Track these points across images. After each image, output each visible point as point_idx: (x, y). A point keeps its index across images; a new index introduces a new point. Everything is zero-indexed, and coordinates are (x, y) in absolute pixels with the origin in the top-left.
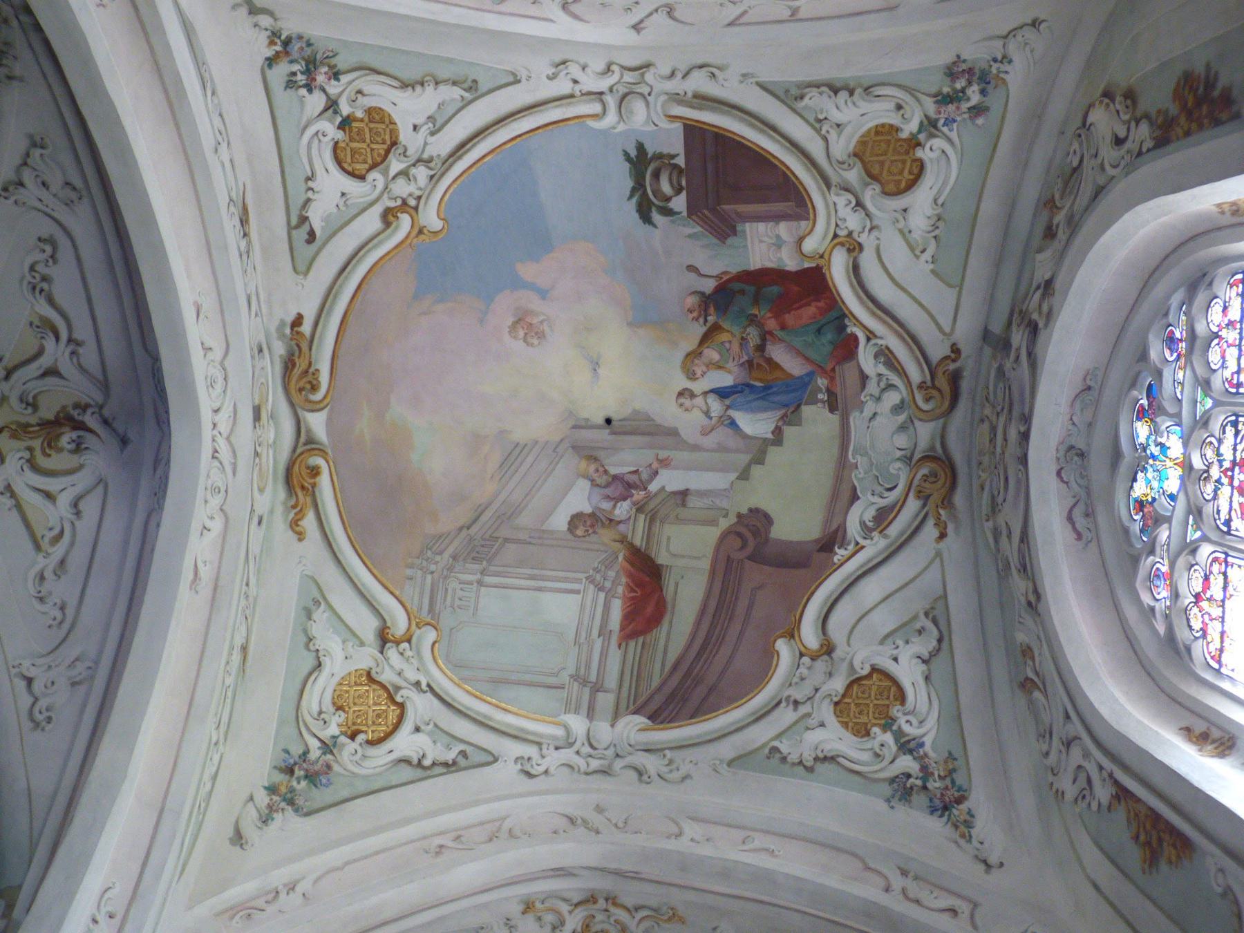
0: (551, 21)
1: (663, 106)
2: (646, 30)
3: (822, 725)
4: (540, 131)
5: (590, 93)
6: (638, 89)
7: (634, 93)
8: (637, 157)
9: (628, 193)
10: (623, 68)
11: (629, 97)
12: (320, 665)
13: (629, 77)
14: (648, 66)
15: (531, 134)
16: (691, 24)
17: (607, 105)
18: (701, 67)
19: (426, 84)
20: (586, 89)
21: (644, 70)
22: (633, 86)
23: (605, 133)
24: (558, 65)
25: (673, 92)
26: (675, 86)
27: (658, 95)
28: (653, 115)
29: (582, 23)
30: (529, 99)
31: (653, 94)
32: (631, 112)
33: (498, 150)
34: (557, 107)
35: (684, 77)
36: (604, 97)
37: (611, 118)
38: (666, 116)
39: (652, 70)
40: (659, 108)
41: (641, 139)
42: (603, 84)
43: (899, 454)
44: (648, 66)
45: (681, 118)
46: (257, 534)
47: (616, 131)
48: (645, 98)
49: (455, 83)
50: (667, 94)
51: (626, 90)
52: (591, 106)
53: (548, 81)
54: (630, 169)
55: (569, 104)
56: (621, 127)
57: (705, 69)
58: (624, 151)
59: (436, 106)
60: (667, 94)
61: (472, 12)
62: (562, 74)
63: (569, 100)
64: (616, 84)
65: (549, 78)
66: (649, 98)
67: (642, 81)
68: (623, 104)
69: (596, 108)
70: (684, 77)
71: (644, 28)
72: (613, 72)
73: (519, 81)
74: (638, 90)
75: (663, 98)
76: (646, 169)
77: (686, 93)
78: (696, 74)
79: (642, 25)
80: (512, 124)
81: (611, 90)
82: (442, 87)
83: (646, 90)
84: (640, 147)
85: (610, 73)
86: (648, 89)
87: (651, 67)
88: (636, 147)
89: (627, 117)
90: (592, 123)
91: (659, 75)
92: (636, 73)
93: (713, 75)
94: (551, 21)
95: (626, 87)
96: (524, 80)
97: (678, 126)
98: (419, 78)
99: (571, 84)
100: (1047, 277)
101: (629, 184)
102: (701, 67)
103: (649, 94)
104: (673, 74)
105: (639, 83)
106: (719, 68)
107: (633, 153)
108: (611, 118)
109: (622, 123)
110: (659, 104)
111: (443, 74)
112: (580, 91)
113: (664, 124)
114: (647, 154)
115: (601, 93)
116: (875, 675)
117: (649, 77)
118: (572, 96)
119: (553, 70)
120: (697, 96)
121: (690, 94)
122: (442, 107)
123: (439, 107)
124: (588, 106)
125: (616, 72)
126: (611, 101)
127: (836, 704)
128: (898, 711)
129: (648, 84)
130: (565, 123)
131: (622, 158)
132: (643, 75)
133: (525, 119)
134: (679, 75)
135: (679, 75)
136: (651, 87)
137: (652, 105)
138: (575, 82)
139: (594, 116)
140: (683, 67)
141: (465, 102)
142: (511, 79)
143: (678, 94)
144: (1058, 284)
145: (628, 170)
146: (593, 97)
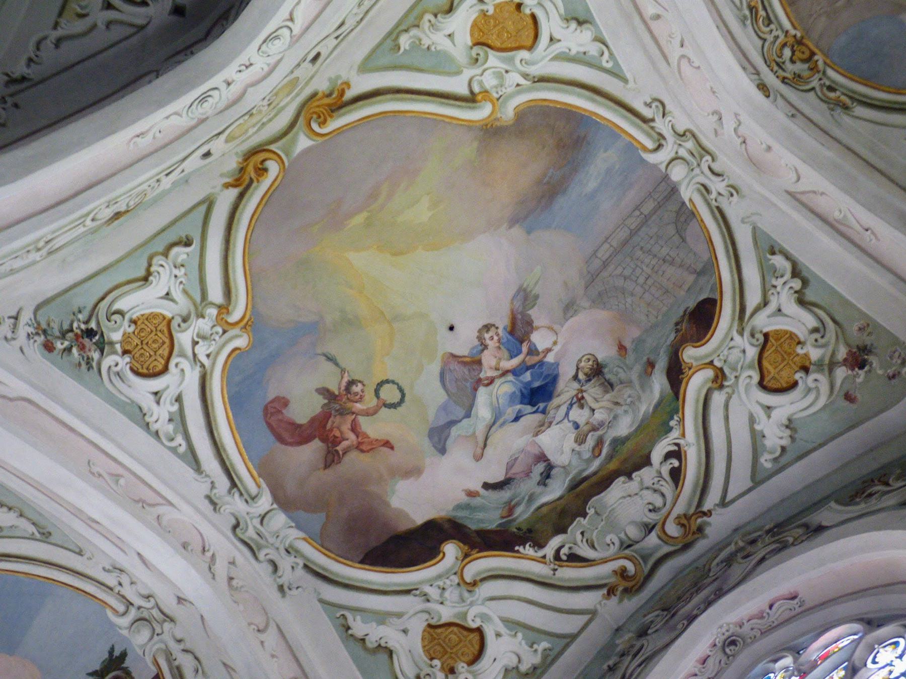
0: (125, 552)
1: (158, 649)
2: (183, 607)
3: (405, 631)
4: (72, 589)
5: (123, 597)
6: (155, 624)
7: (150, 623)
8: (116, 657)
9: (90, 671)
10: (157, 605)
11: (145, 622)
12: (146, 279)
13: (155, 612)
14: (172, 620)
15: (64, 585)
16: (208, 636)
17: (127, 614)
18: (196, 658)
19: (12, 511)
20: (123, 592)
21: (168, 619)
22: (153, 620)
23: (112, 625)
24: (115, 568)
25: (171, 650)
26: (175, 648)
27: (162, 641)
28: (148, 647)
29: (147, 569)
30: (79, 567)
31: (160, 637)
32: (139, 631)
33: (31, 577)
34: (96, 586)
35: (184, 650)
36: (131, 607)
37: (124, 622)
38: (154, 656)
39: (172, 625)
40: (154, 649)
41: (128, 652)
42: (138, 601)
43: (622, 535)
44: (172, 620)
45: (160, 669)
46: (195, 162)
47: (120, 631)
48: (154, 633)
49: (34, 524)
50: (167, 647)
51: (147, 617)
52: (119, 604)
53: (102, 570)
54: (106, 659)
55: (105, 591)
56: (125, 632)
57: (197, 662)
58: (113, 646)
59: (10, 524)
60: (167, 647)
61: (68, 513)
62: (115, 574)
63: (107, 590)
64: (145, 608)
65: (104, 569)
66: (155, 635)
67: (161, 623)
68: (138, 622)
69: (121, 608)
70: (184, 650)
71: (184, 605)
72: (149, 601)
73: (82, 555)
74: (154, 625)
75: (163, 646)
76: (114, 670)
77: (175, 660)
78: (190, 657)
79: (184, 602)
80: (55, 571)
81: (139, 608)
82: (23, 520)
83: (158, 630)
84: (124, 655)
85: (147, 600)
86: (160, 632)
87: (172, 623)
88: (122, 652)
89: (134, 631)
90: (109, 613)
91: (172, 632)
92: (162, 616)
93: (197, 671)
94: (125, 552)
95: (149, 616)
96: (85, 557)
97: (154, 670)
98: (10, 505)
99: (116, 583)
100: (824, 523)
101: (97, 667)
102: (196, 658)
103: (158, 635)
104: (179, 641)
105: (158, 622)
106: (203, 672)
107: (117, 653)
108: (124, 622)
109: (128, 630)
110: (156, 647)
111: (28, 513)
112: (119, 591)
113: (149, 659)
114: (123, 663)
115: (132, 604)
116: (472, 636)
117: (167, 626)
118: (111, 589)
119: (111, 568)
120: (178, 668)
121: (176, 663)
122: (13, 528)
123: (11, 527)
124: (116, 602)
125: (150, 603)
126: (133, 613)
127: (430, 626)
128: (463, 667)
129: (162, 628)
130: (93, 598)
131: (108, 648)
132: (165, 621)
133: (68, 575)
134: (182, 646)
135: (182, 646)
136: (163, 632)
137: (153, 642)
138: (120, 584)
139: (115, 611)
140: (188, 646)
141: (32, 537)
142: (77, 550)
143: (172, 655)
144: (826, 534)
145: (104, 659)
146: (124, 601)
